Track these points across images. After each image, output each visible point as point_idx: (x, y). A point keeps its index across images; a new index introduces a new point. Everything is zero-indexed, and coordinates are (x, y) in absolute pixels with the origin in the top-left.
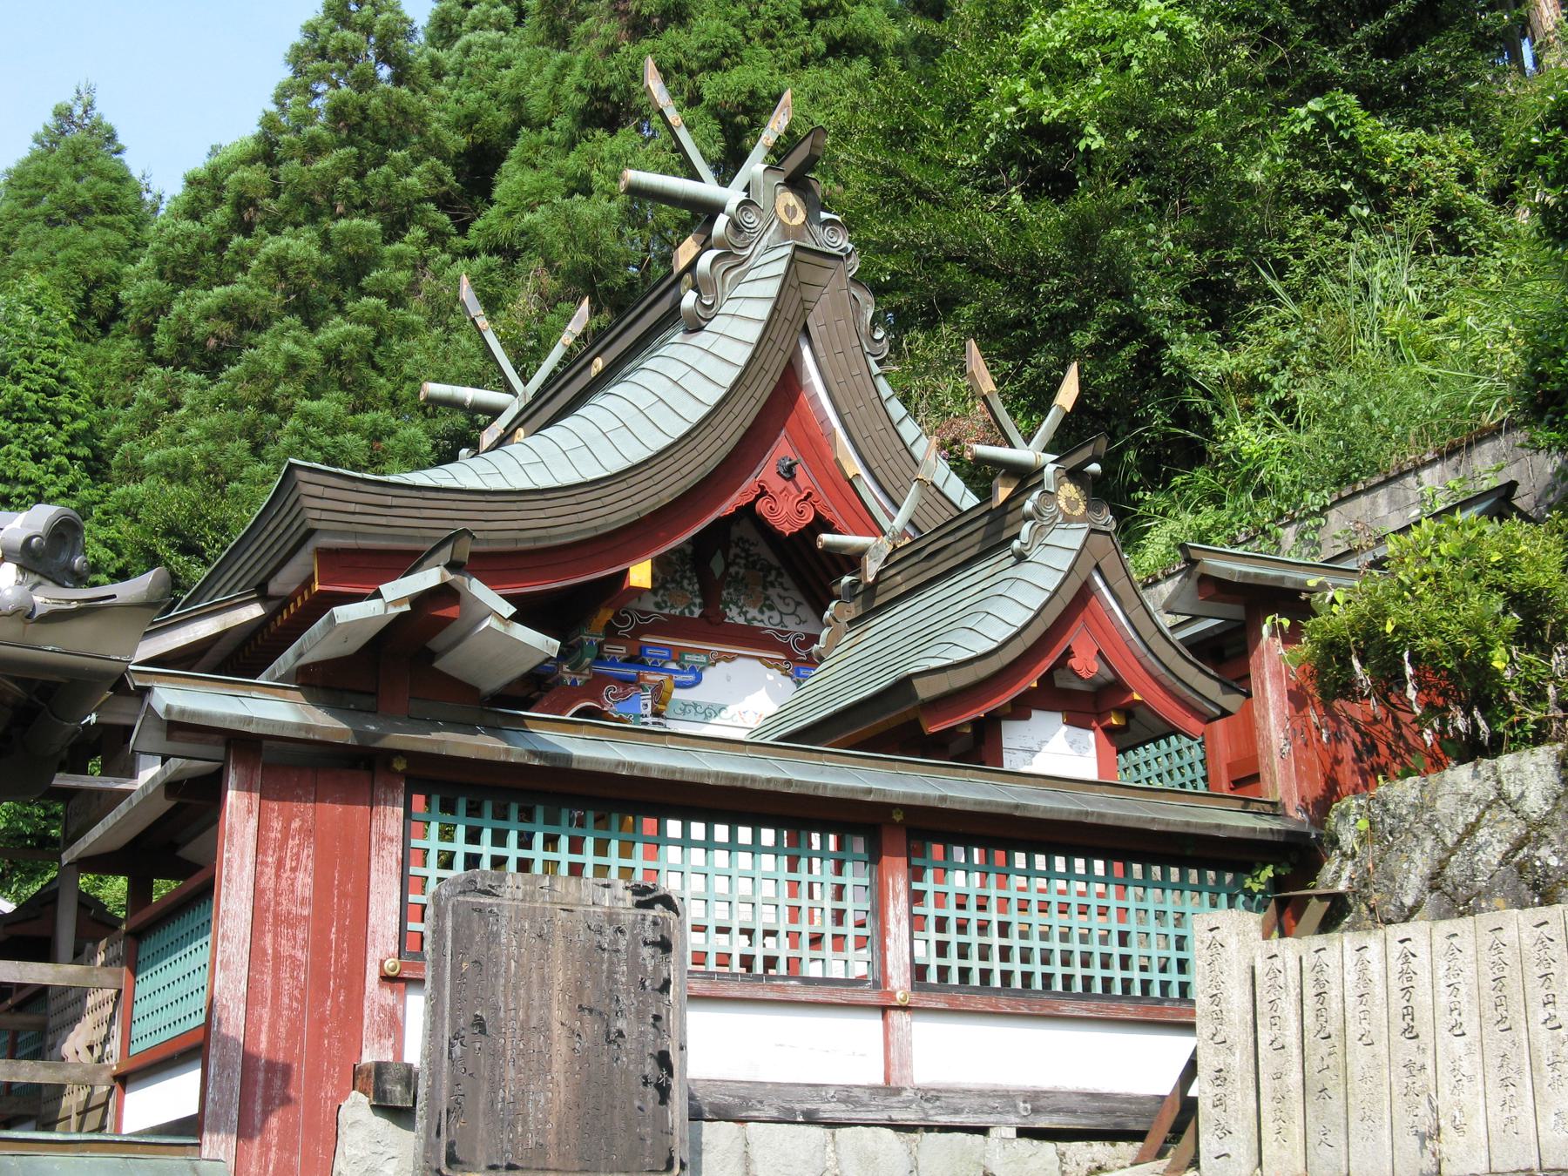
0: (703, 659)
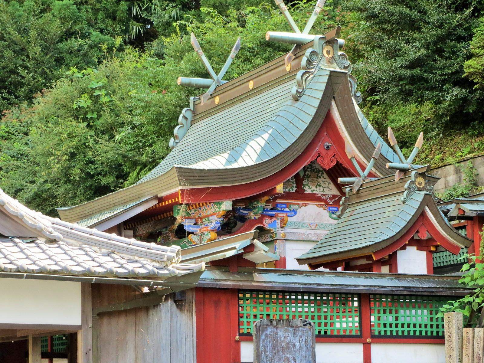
0: (297, 206)
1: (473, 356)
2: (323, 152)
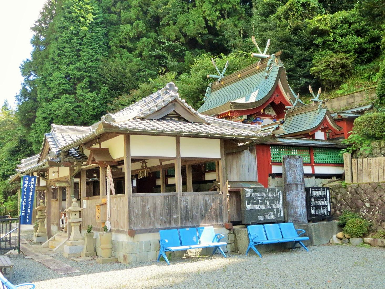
1: (358, 170)
2: (276, 98)
